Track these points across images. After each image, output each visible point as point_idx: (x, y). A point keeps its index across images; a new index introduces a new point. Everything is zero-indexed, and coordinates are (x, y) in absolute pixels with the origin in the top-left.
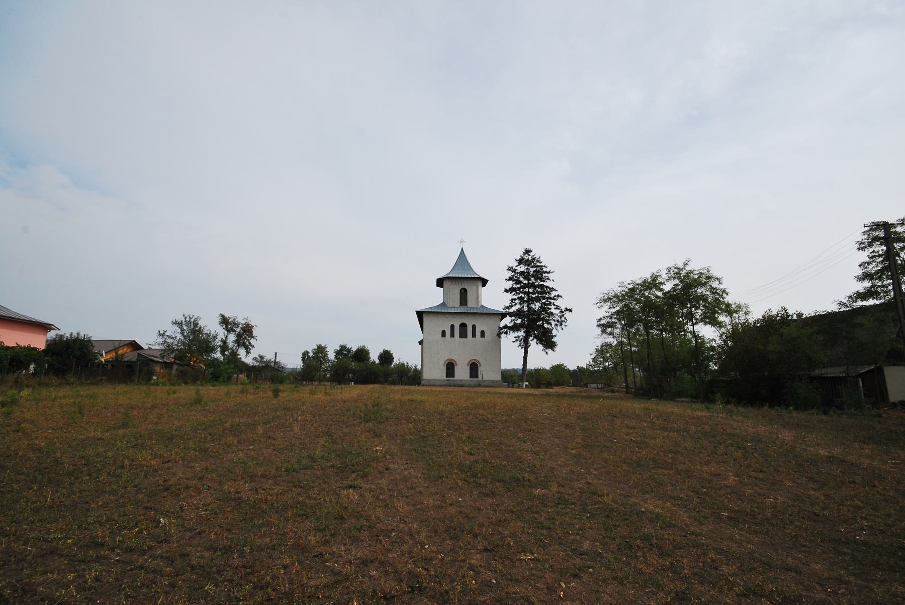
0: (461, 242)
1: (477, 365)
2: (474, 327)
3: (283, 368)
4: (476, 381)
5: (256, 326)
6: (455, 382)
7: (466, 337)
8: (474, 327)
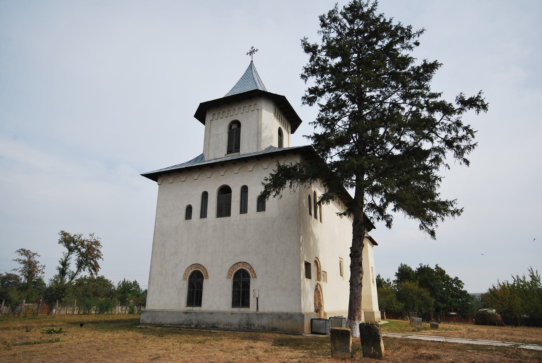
1: (248, 276)
2: (244, 190)
4: (242, 314)
5: (281, 196)
6: (200, 318)
7: (228, 214)
8: (244, 190)
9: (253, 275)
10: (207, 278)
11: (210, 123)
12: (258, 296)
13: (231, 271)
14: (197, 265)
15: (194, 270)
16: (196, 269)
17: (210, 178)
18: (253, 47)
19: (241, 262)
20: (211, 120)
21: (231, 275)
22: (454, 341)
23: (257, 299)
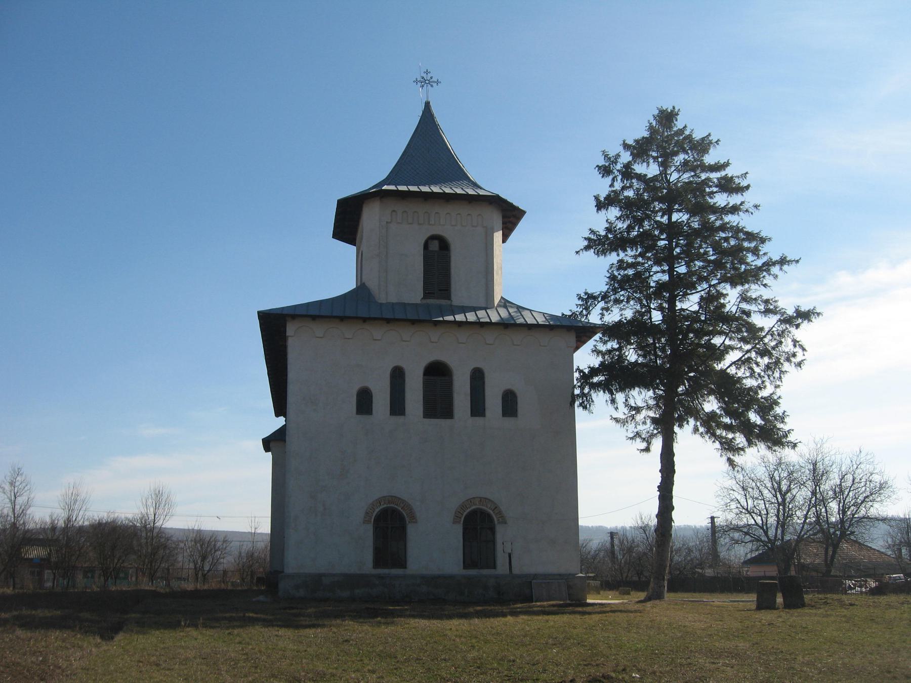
0: (426, 82)
1: (402, 519)
2: (478, 377)
3: (168, 539)
8: (478, 377)
9: (500, 519)
10: (414, 520)
12: (510, 552)
13: (459, 512)
15: (385, 506)
16: (388, 505)
21: (460, 518)
22: (534, 606)
23: (510, 555)
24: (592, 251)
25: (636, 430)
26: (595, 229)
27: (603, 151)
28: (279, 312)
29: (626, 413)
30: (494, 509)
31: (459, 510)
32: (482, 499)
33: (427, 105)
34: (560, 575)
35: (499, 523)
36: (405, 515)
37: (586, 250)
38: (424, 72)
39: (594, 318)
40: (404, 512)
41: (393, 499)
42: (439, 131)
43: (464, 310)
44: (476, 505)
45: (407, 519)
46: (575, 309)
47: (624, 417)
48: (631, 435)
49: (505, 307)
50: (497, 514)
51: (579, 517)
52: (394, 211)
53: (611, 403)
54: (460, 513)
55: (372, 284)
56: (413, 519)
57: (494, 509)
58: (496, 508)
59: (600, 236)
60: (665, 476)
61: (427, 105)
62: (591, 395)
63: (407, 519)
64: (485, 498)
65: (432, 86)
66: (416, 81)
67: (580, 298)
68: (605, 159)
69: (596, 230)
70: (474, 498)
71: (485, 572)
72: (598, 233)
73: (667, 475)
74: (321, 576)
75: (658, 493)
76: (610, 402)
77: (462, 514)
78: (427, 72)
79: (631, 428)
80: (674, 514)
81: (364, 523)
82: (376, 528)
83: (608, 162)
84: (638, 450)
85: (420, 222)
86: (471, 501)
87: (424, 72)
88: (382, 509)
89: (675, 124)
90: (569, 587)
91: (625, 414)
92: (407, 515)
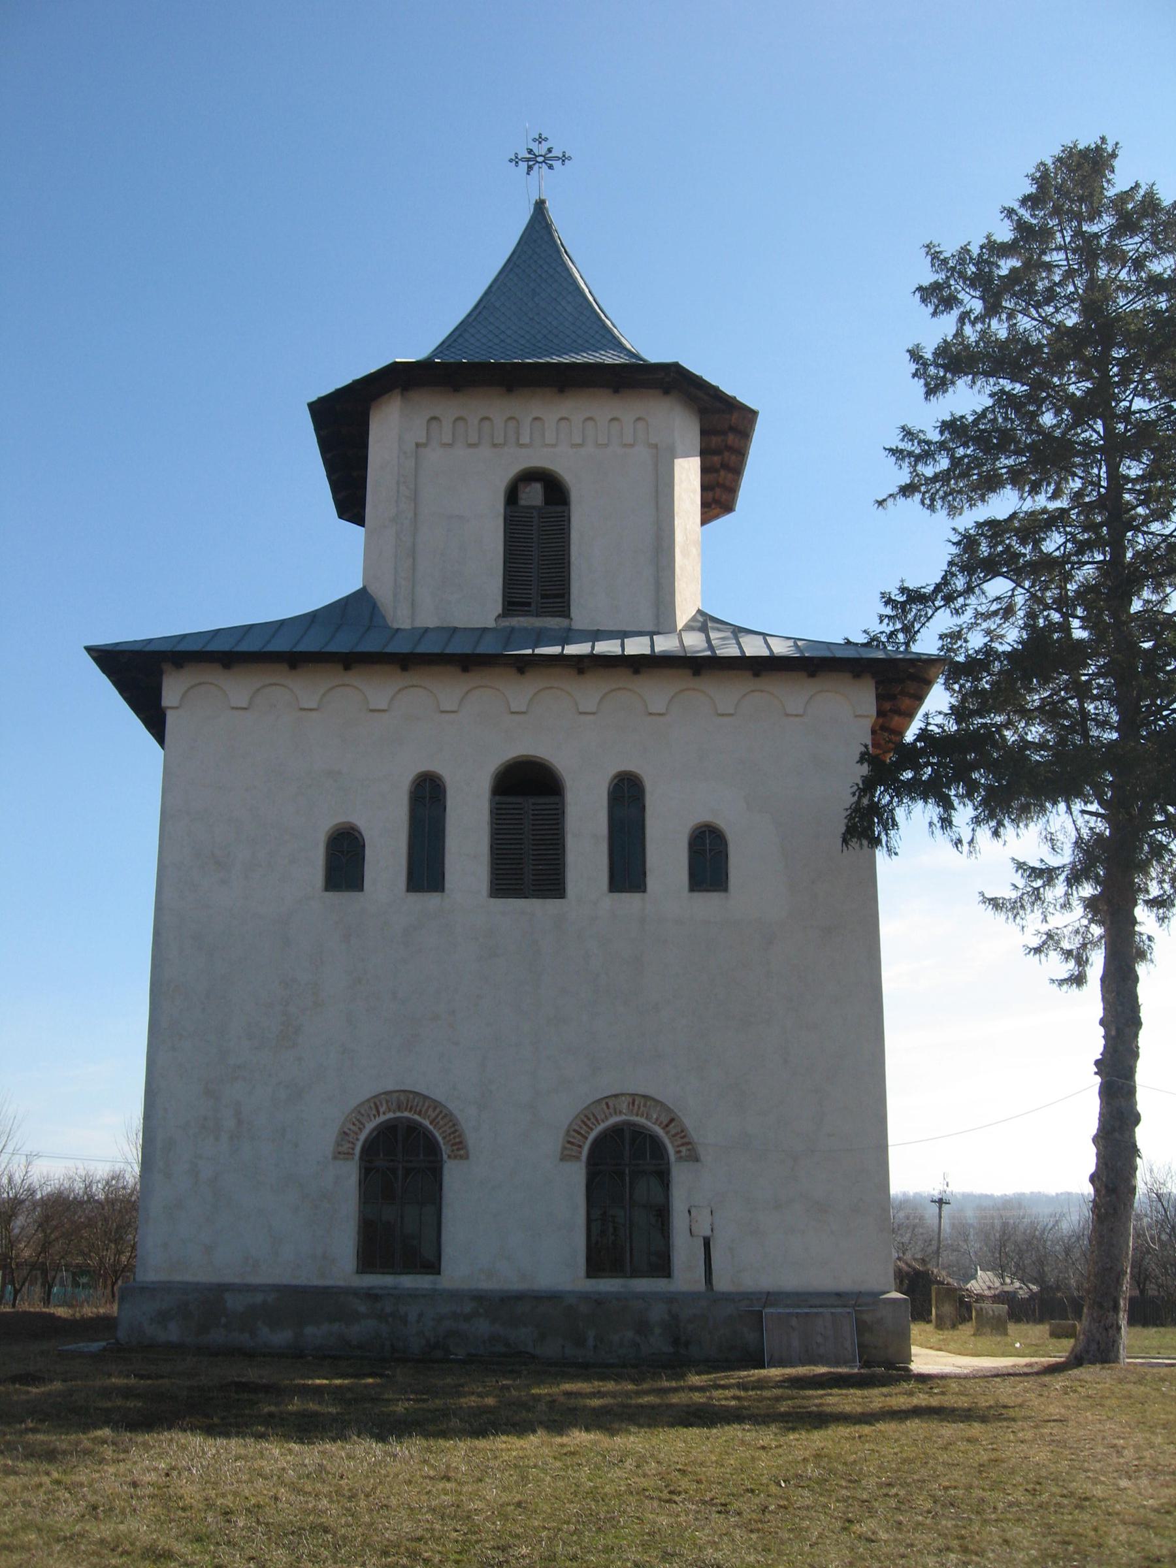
1: (432, 1148)
9: (683, 1149)
10: (462, 1152)
11: (417, 458)
12: (708, 1233)
13: (575, 1131)
14: (411, 1096)
15: (391, 1115)
16: (398, 1114)
17: (453, 715)
18: (546, 139)
19: (622, 1094)
20: (418, 445)
21: (580, 1146)
23: (707, 1243)
24: (918, 497)
25: (1044, 928)
26: (915, 425)
27: (928, 246)
28: (137, 648)
29: (1021, 886)
30: (667, 1126)
31: (577, 1128)
32: (636, 1097)
33: (540, 206)
34: (838, 1295)
35: (680, 1159)
36: (440, 1139)
37: (904, 495)
38: (534, 140)
39: (927, 643)
40: (437, 1134)
41: (411, 1098)
42: (558, 251)
43: (596, 636)
44: (621, 1112)
45: (445, 1149)
46: (876, 628)
47: (1014, 895)
48: (1035, 942)
49: (704, 629)
50: (674, 1136)
51: (890, 1142)
52: (434, 418)
53: (942, 827)
54: (579, 1133)
55: (383, 594)
56: (460, 1148)
57: (667, 1126)
58: (672, 1120)
59: (928, 443)
60: (1113, 1033)
61: (540, 206)
62: (892, 811)
63: (443, 1147)
64: (644, 1096)
65: (551, 167)
66: (516, 160)
67: (889, 601)
68: (933, 265)
69: (918, 428)
70: (616, 1096)
71: (643, 1285)
72: (922, 436)
73: (1118, 1029)
74: (222, 1289)
75: (1098, 1079)
76: (939, 825)
77: (586, 1138)
78: (540, 139)
79: (1034, 923)
80: (1143, 1135)
81: (335, 1158)
82: (367, 1171)
83: (942, 270)
84: (1053, 981)
85: (496, 442)
86: (607, 1104)
87: (534, 140)
88: (381, 1124)
89: (1108, 181)
90: (862, 1327)
91: (1016, 887)
92: (444, 1138)
